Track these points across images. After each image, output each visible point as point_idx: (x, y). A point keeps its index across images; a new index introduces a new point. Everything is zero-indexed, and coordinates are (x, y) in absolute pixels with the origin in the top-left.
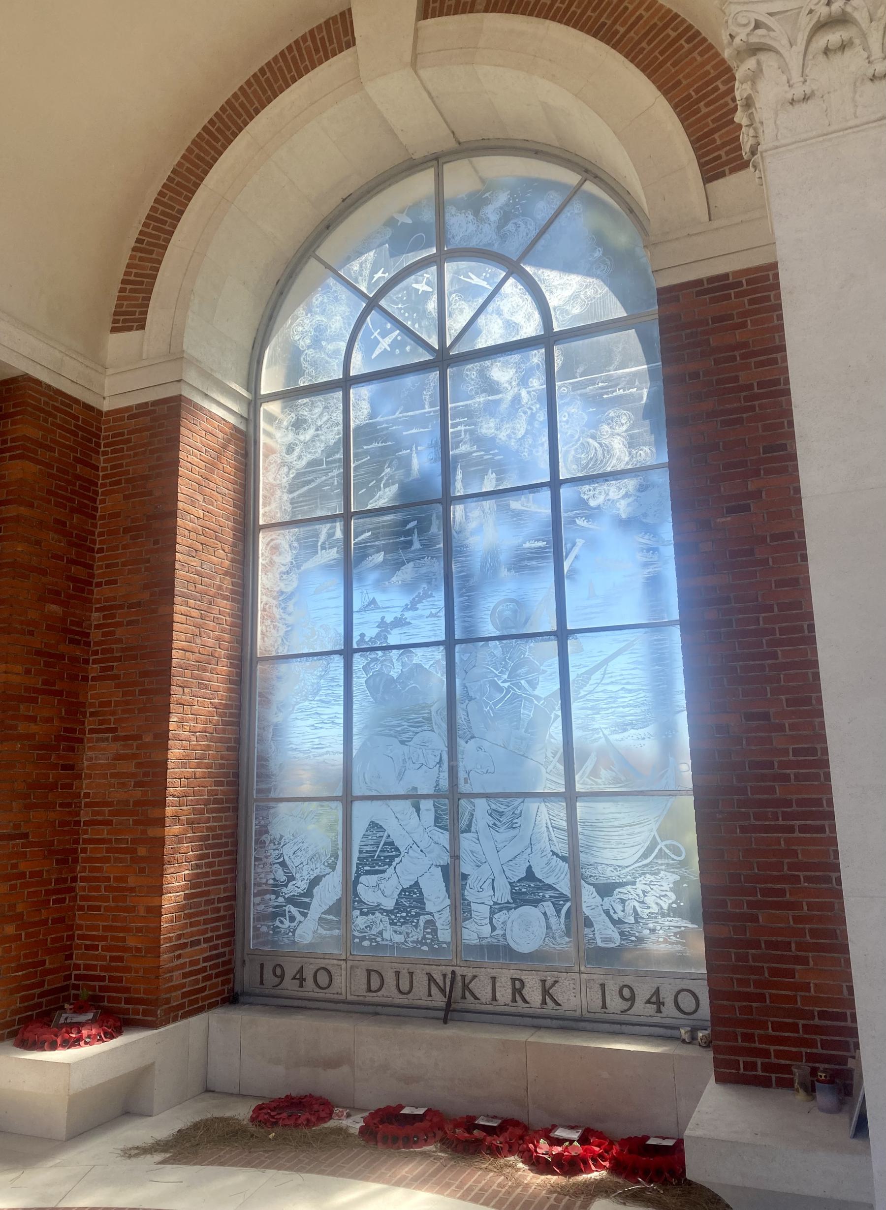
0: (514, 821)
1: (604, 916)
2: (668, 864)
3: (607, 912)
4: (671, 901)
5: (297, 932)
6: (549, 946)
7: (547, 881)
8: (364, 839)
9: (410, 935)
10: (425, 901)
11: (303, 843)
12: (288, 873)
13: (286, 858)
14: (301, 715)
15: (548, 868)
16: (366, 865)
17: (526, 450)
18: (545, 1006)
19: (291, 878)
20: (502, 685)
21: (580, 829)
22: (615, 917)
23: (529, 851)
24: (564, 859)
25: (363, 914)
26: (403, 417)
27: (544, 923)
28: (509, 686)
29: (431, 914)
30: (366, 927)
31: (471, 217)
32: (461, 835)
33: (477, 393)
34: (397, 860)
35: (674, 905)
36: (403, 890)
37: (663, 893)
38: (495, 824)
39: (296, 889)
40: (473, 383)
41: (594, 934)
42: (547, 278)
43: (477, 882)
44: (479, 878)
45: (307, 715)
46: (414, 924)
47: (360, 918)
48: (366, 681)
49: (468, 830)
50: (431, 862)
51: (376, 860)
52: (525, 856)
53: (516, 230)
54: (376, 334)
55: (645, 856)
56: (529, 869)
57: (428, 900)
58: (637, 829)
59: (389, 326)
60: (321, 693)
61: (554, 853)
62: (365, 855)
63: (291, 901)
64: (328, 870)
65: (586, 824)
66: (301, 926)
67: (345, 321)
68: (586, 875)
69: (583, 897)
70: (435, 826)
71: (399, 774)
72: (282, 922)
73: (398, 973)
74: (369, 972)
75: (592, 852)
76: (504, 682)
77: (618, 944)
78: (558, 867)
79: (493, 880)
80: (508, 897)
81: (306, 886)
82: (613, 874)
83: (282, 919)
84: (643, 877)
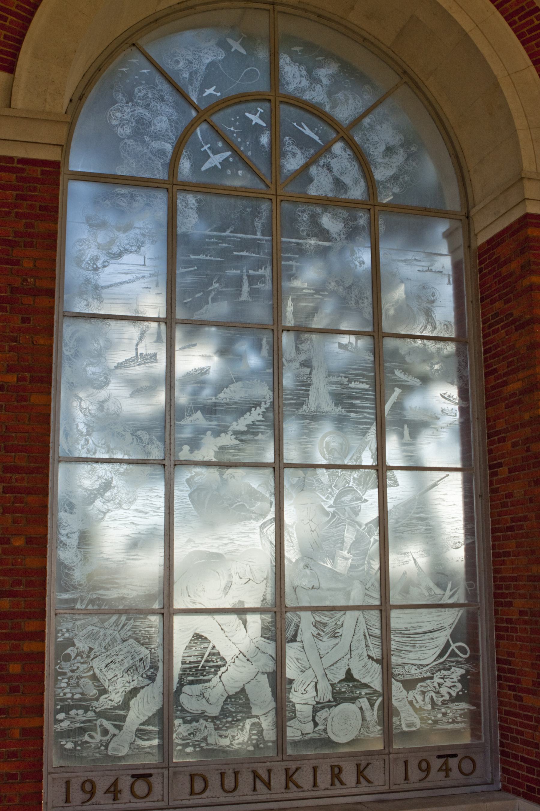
0: (337, 631)
1: (408, 706)
2: (457, 662)
3: (411, 703)
4: (458, 690)
5: (111, 746)
6: (364, 735)
7: (363, 681)
8: (187, 651)
9: (236, 738)
10: (251, 705)
11: (117, 655)
12: (99, 686)
13: (97, 671)
14: (112, 524)
15: (364, 670)
16: (189, 675)
17: (353, 299)
18: (359, 785)
19: (103, 691)
20: (328, 509)
21: (392, 637)
22: (417, 706)
23: (349, 656)
24: (377, 661)
25: (185, 722)
26: (233, 237)
27: (360, 716)
28: (334, 512)
29: (257, 717)
30: (190, 734)
31: (304, 73)
32: (287, 644)
33: (308, 235)
34: (223, 669)
35: (461, 693)
36: (229, 697)
37: (453, 684)
38: (319, 634)
39: (110, 702)
40: (304, 224)
41: (400, 722)
42: (372, 153)
43: (302, 685)
44: (303, 682)
45: (121, 524)
46: (240, 727)
47: (183, 726)
48: (190, 495)
49: (294, 639)
50: (257, 670)
51: (201, 670)
52: (345, 660)
53: (346, 101)
54: (206, 147)
55: (441, 655)
56: (349, 672)
57: (254, 704)
58: (436, 634)
59: (220, 144)
60: (138, 502)
61: (370, 657)
62: (188, 666)
63: (102, 714)
64: (147, 682)
65: (397, 632)
66: (115, 739)
67: (173, 124)
68: (395, 673)
69: (393, 692)
70: (262, 636)
71: (225, 588)
72: (92, 737)
73: (222, 774)
74: (192, 777)
75: (401, 655)
76: (329, 507)
77: (418, 727)
78: (373, 668)
79: (316, 683)
80: (329, 697)
81: (121, 699)
82: (416, 672)
83: (92, 733)
84: (439, 673)
